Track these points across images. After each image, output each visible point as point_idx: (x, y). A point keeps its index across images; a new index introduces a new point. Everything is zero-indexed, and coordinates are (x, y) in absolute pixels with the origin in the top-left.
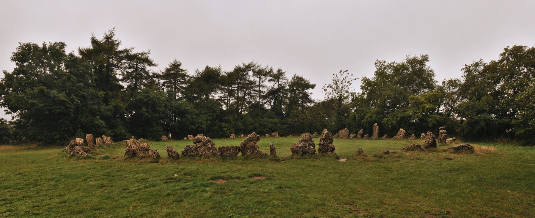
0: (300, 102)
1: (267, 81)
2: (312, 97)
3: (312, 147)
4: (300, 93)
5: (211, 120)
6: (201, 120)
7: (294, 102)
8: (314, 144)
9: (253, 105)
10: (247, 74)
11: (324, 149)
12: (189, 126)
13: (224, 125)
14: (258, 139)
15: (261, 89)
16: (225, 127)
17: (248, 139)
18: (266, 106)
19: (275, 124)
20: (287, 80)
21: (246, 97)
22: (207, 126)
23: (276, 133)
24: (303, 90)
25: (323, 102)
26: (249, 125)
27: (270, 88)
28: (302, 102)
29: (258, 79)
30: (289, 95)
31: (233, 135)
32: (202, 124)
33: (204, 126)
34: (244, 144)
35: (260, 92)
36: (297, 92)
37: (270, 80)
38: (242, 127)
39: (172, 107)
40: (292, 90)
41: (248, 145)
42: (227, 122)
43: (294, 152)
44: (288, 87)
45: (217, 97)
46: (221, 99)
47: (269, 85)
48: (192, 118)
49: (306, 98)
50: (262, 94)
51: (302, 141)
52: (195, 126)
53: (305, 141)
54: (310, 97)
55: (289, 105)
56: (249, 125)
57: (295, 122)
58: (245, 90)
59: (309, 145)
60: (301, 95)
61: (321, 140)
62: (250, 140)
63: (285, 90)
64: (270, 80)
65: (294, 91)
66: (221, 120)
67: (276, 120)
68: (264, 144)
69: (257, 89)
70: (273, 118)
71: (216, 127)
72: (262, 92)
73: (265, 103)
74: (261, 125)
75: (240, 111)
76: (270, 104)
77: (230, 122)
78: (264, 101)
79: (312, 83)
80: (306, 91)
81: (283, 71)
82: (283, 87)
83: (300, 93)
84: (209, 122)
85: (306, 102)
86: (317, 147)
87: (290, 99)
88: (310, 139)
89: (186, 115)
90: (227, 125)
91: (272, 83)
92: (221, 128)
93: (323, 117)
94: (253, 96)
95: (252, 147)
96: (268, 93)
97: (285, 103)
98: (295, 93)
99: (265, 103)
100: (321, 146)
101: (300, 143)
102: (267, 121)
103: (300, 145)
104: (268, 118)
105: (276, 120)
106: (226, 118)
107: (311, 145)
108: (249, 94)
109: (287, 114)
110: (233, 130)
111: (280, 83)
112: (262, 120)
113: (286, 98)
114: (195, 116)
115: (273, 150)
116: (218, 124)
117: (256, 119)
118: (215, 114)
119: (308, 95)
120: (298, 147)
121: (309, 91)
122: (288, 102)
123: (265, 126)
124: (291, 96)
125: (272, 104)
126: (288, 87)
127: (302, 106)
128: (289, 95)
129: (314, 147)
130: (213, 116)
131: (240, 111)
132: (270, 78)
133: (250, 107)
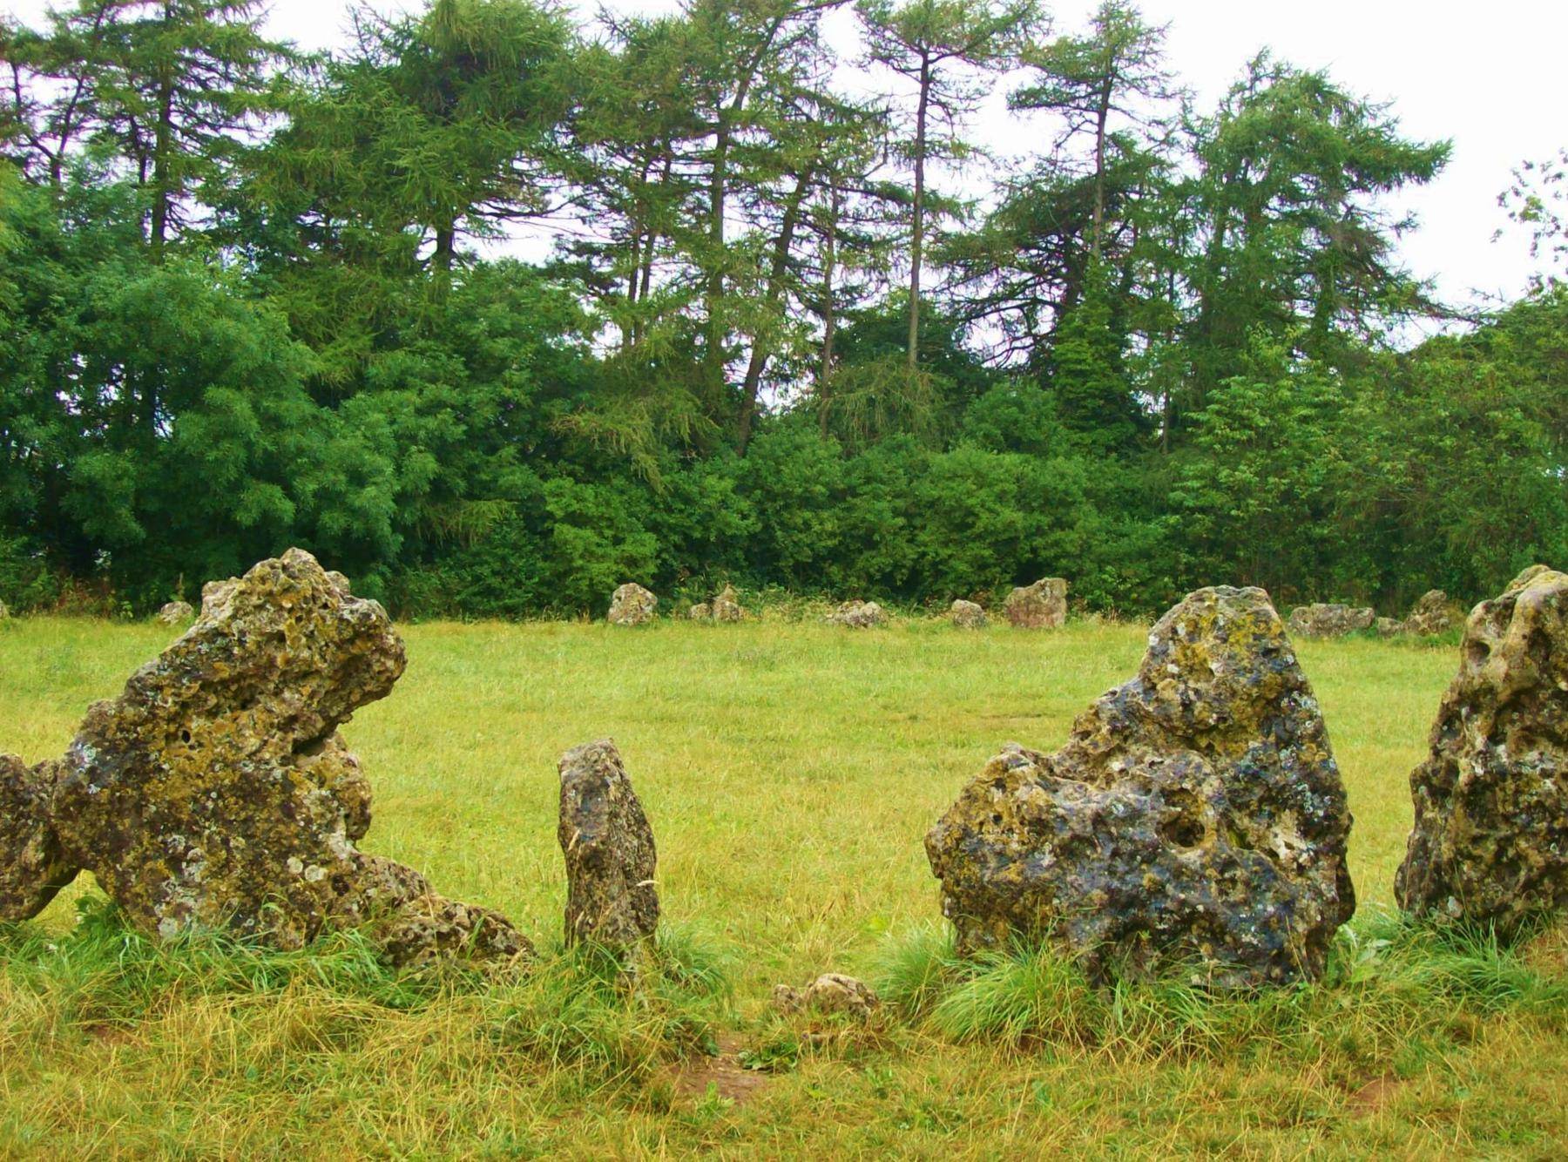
0: (1303, 310)
1: (996, 103)
2: (1403, 257)
3: (1286, 839)
4: (1309, 219)
5: (442, 449)
6: (348, 442)
7: (1239, 308)
8: (1328, 787)
9: (866, 322)
10: (808, 36)
11: (1504, 865)
12: (236, 487)
13: (560, 492)
14: (360, 673)
15: (938, 177)
16: (576, 519)
17: (181, 665)
18: (984, 337)
19: (1056, 504)
20: (1185, 98)
21: (801, 251)
22: (401, 498)
23: (1055, 587)
24: (1333, 189)
25: (1521, 310)
26: (807, 502)
27: (1028, 167)
28: (1325, 308)
29: (901, 91)
30: (1199, 242)
31: (631, 598)
32: (358, 479)
33: (376, 498)
34: (125, 743)
35: (925, 203)
36: (1274, 206)
37: (1023, 101)
38: (740, 520)
39: (87, 318)
40: (1227, 194)
41: (172, 760)
42: (596, 465)
43: (986, 905)
44: (1186, 167)
45: (527, 243)
46: (577, 269)
47: (1003, 143)
48: (273, 422)
49: (1355, 264)
50: (949, 225)
51: (1127, 723)
52: (290, 494)
53: (1190, 733)
54: (1392, 262)
55: (1198, 332)
56: (807, 502)
57: (1240, 492)
58: (789, 185)
59: (1233, 801)
60: (1310, 238)
61: (1449, 720)
62: (226, 679)
63: (1167, 191)
64: (1023, 101)
65: (1251, 202)
66: (550, 450)
67: (1068, 468)
68: (466, 747)
69: (897, 174)
70: (1037, 449)
71: (490, 510)
72: (951, 207)
73: (977, 310)
74: (914, 514)
75: (739, 373)
76: (1030, 318)
77: (623, 463)
78: (964, 292)
79: (1412, 133)
80: (1357, 199)
81: (1148, 20)
82: (1148, 161)
83: (1309, 219)
84: (425, 463)
85: (1358, 305)
86: (1375, 865)
87: (1204, 273)
88: (1278, 703)
89: (214, 394)
90: (590, 498)
91: (1049, 122)
92: (535, 522)
93: (1517, 446)
94: (861, 242)
95: (250, 791)
96: (1003, 214)
97: (1157, 318)
98: (1255, 221)
99: (977, 310)
100: (1453, 819)
101: (1091, 764)
102: (982, 480)
103: (1079, 801)
104: (989, 442)
105: (1068, 468)
106: (584, 422)
107: (1277, 800)
108: (825, 225)
109: (1173, 416)
110: (648, 544)
111: (1115, 123)
112: (939, 460)
113: (1168, 260)
114: (299, 405)
115: (605, 846)
116: (517, 477)
117: (872, 454)
118: (480, 394)
119: (1373, 242)
120: (1040, 825)
121: (1379, 207)
122: (1188, 301)
123: (960, 523)
124: (1216, 253)
125: (1046, 320)
126: (1186, 167)
127: (1321, 343)
128: (1199, 242)
129: (1329, 831)
130: (463, 412)
131: (739, 373)
132: (1029, 77)
133: (840, 345)
